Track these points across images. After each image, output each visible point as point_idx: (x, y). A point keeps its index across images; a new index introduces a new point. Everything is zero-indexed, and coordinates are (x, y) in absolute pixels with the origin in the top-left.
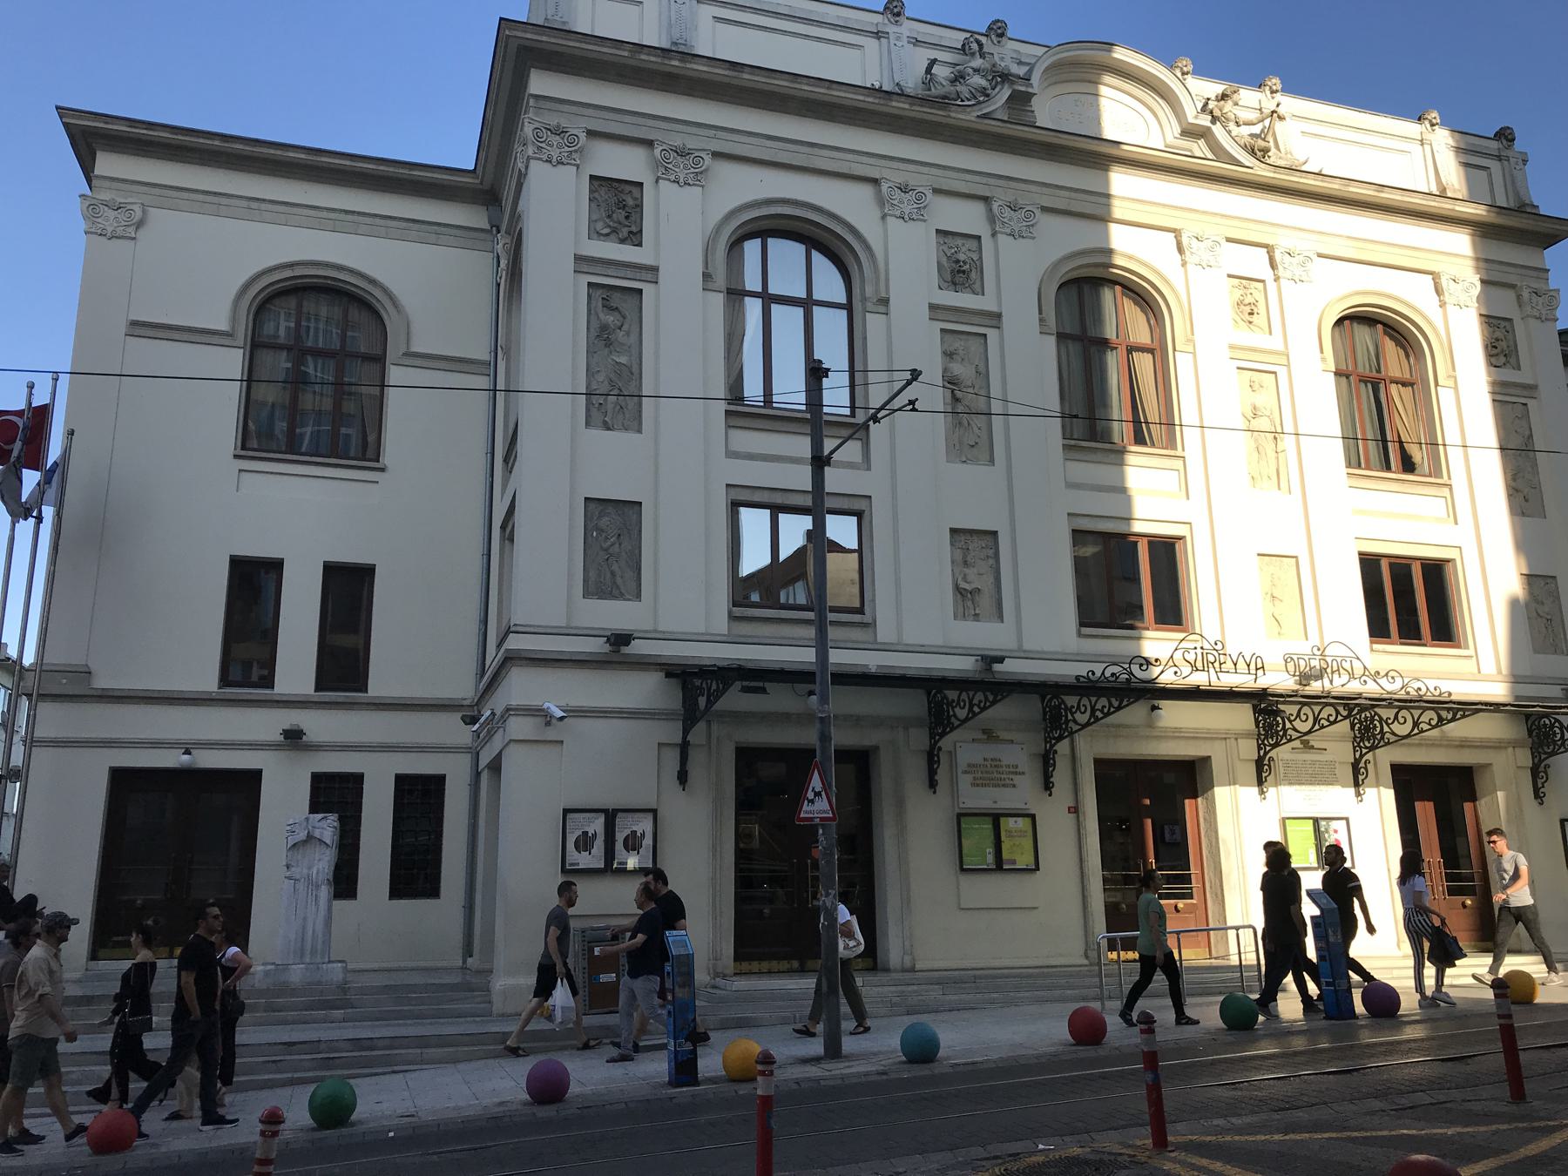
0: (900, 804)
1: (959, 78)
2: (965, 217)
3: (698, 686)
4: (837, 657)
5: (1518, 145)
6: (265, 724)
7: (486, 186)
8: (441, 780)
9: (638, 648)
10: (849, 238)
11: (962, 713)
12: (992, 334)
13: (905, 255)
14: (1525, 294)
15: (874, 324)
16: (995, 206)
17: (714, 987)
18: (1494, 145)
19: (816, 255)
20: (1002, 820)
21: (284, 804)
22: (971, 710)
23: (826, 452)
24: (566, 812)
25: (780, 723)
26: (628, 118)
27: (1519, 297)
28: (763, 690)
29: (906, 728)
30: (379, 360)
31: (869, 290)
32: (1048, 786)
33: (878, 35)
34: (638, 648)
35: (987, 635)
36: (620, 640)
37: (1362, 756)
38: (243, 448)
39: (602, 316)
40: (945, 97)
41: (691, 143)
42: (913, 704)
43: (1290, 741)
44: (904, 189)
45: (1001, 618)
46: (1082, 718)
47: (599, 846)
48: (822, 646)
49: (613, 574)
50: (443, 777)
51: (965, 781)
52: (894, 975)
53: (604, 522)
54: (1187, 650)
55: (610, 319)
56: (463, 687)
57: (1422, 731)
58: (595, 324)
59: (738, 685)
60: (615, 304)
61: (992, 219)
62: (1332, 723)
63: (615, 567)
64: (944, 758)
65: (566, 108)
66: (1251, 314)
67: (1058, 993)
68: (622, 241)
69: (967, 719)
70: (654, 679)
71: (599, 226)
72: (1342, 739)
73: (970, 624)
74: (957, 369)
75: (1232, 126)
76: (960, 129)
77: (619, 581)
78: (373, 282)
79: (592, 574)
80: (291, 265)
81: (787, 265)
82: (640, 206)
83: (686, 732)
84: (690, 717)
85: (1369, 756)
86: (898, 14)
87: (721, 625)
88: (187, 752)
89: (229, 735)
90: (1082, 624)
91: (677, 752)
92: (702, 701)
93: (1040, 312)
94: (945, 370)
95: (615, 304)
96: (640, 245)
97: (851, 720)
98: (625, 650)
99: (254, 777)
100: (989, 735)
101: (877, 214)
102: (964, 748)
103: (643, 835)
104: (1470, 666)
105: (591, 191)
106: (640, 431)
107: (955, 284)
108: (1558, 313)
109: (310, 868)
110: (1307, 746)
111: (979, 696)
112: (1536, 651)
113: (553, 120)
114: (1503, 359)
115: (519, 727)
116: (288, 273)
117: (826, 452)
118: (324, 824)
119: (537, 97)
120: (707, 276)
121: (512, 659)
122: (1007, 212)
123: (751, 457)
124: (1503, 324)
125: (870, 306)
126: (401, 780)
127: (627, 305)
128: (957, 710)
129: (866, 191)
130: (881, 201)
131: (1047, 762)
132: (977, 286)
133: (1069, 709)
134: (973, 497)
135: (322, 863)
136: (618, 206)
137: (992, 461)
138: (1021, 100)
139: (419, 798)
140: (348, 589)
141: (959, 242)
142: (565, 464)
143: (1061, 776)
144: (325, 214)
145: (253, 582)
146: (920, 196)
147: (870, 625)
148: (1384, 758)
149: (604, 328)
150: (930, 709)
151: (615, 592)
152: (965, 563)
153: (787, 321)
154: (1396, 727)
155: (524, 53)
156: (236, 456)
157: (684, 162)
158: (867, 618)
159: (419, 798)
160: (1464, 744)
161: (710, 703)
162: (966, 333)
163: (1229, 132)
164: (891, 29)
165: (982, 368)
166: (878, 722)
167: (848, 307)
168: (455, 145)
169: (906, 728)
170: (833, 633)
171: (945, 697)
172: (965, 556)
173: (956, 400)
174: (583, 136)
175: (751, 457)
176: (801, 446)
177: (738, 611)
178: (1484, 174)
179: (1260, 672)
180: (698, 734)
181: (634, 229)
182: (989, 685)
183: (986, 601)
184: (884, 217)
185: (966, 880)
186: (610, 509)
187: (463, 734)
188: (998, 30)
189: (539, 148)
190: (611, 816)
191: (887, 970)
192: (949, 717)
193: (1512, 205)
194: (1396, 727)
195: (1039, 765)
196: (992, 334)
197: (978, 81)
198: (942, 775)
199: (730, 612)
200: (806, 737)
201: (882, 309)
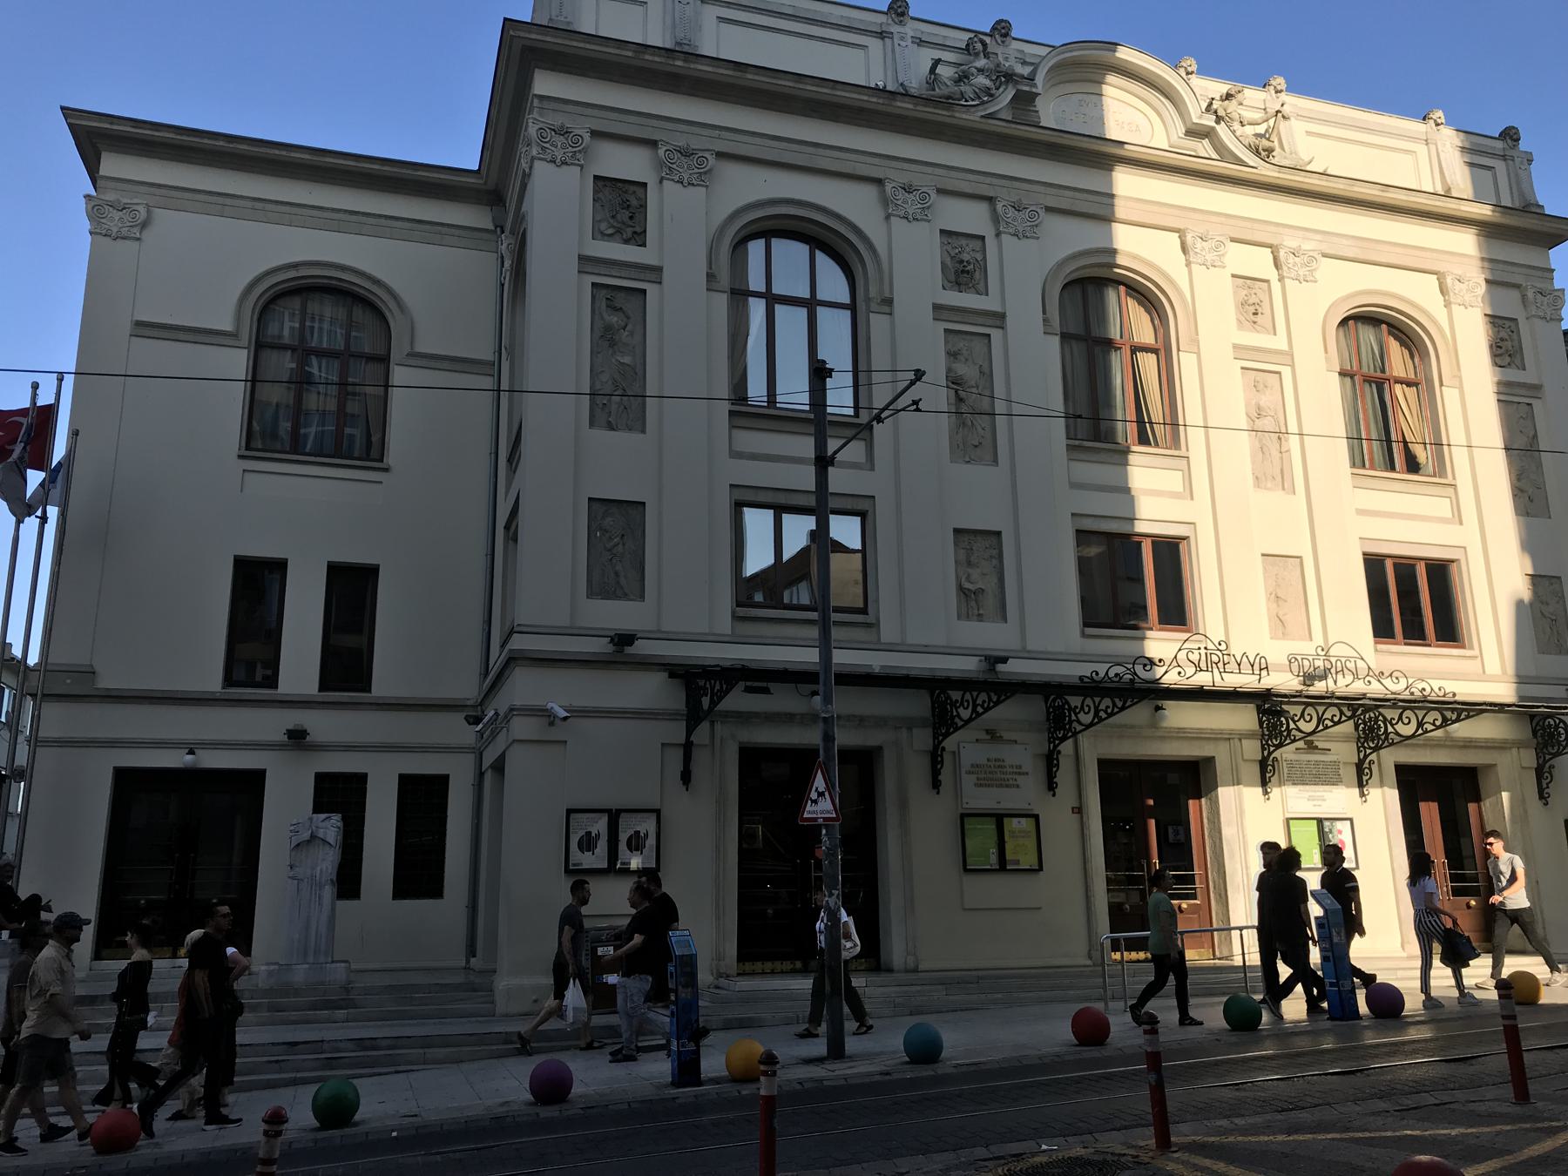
0: (903, 805)
3: (702, 687)
4: (841, 658)
6: (272, 724)
8: (444, 780)
9: (642, 648)
12: (996, 334)
13: (911, 258)
15: (878, 324)
16: (999, 206)
17: (717, 987)
18: (1499, 145)
19: (820, 255)
21: (287, 805)
22: (974, 710)
24: (569, 812)
26: (632, 119)
27: (994, 210)
28: (766, 691)
29: (910, 729)
30: (384, 360)
31: (873, 292)
32: (1051, 786)
34: (642, 648)
35: (990, 635)
36: (624, 640)
37: (1366, 756)
38: (248, 448)
39: (606, 316)
41: (695, 143)
42: (917, 705)
43: (1294, 741)
44: (908, 189)
46: (1086, 718)
49: (617, 574)
51: (968, 782)
54: (1191, 650)
55: (614, 319)
56: (467, 688)
57: (1426, 732)
59: (741, 685)
60: (619, 304)
61: (996, 219)
62: (1336, 724)
63: (619, 567)
64: (947, 758)
65: (570, 108)
68: (626, 242)
69: (970, 720)
71: (603, 226)
72: (1345, 739)
74: (961, 369)
77: (623, 581)
80: (295, 266)
81: (790, 264)
82: (644, 206)
83: (689, 732)
84: (694, 716)
85: (1373, 757)
87: (725, 625)
88: (191, 752)
89: (228, 737)
92: (706, 701)
94: (949, 370)
95: (619, 304)
98: (629, 650)
100: (993, 735)
102: (966, 746)
103: (598, 836)
104: (1473, 666)
106: (643, 431)
107: (959, 284)
110: (1311, 747)
113: (557, 120)
114: (1508, 359)
115: (521, 727)
116: (292, 274)
117: (830, 453)
119: (541, 98)
120: (711, 277)
124: (1508, 324)
125: (874, 306)
128: (961, 710)
129: (870, 191)
130: (885, 201)
131: (1051, 761)
132: (981, 287)
133: (954, 704)
136: (622, 207)
137: (995, 461)
138: (1025, 101)
139: (422, 799)
140: (352, 589)
141: (963, 242)
145: (257, 582)
146: (924, 196)
147: (873, 626)
148: (1389, 758)
149: (608, 328)
153: (791, 322)
154: (1400, 728)
155: (525, 52)
156: (240, 457)
157: (691, 162)
158: (870, 619)
160: (1468, 744)
161: (713, 703)
163: (1234, 132)
164: (895, 29)
165: (987, 371)
166: (881, 722)
167: (852, 307)
169: (910, 729)
170: (836, 633)
171: (949, 697)
173: (960, 400)
178: (1409, 157)
179: (1264, 673)
180: (702, 733)
181: (638, 229)
182: (993, 685)
183: (990, 601)
184: (888, 217)
185: (970, 880)
188: (1002, 29)
189: (544, 149)
190: (614, 816)
191: (890, 970)
192: (953, 718)
196: (996, 334)
197: (982, 80)
198: (946, 776)
199: (733, 613)
200: (811, 737)
201: (887, 309)
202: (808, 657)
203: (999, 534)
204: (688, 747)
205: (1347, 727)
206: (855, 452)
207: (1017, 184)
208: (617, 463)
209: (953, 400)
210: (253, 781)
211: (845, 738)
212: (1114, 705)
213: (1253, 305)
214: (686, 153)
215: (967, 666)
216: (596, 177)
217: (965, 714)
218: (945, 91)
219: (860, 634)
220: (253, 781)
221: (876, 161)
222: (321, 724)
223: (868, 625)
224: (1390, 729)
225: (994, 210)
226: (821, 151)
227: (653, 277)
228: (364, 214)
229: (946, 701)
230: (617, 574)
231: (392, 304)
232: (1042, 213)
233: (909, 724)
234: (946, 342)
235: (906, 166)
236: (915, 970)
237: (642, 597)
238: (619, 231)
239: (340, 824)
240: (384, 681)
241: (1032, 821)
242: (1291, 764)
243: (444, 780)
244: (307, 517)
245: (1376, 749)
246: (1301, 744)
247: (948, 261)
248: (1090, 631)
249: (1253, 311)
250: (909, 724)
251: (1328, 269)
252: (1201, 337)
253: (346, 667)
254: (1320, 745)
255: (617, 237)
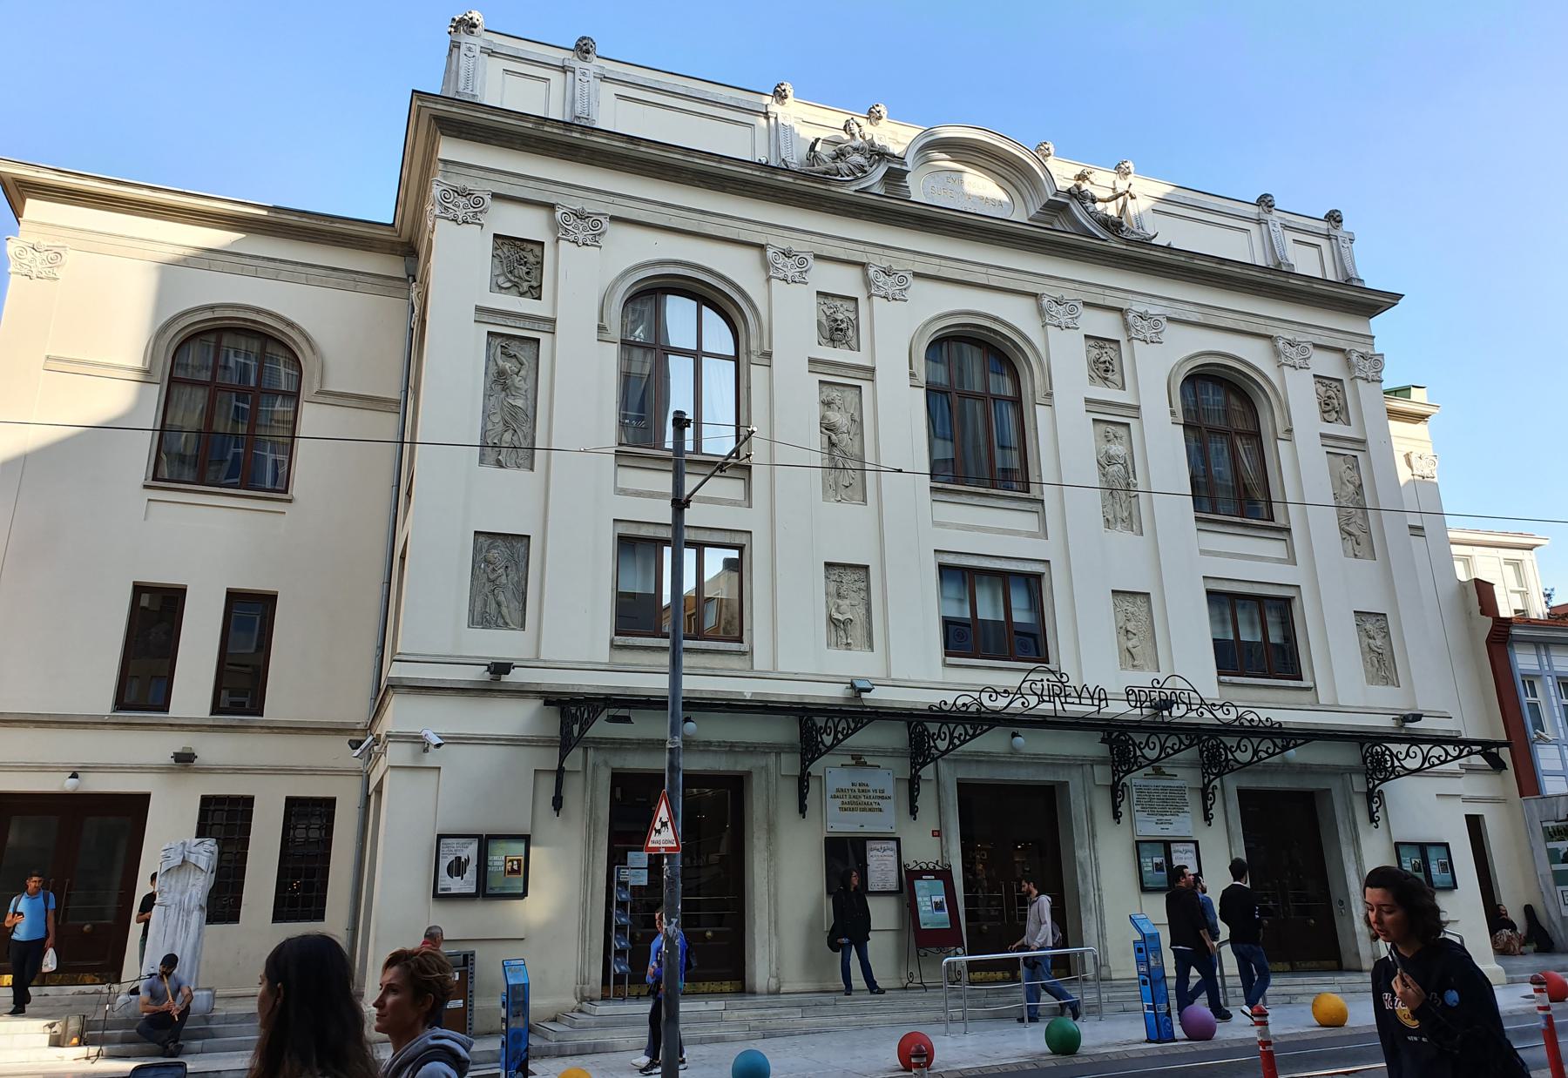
0: (771, 829)
1: (840, 155)
2: (845, 281)
3: (573, 712)
4: (689, 684)
5: (1346, 226)
6: (159, 746)
7: (404, 239)
8: (331, 802)
9: (515, 677)
10: (736, 297)
11: (828, 740)
12: (865, 385)
13: (790, 317)
14: (1354, 357)
15: (757, 374)
16: (871, 272)
17: (580, 1011)
18: (1324, 225)
19: (709, 314)
20: (1174, 847)
21: (170, 832)
22: (951, 742)
23: (687, 492)
24: (440, 837)
25: (647, 744)
26: (531, 183)
27: (1125, 320)
28: (627, 720)
29: (778, 754)
30: (294, 396)
31: (754, 345)
32: (913, 811)
33: (564, 69)
34: (515, 677)
35: (856, 664)
36: (500, 669)
37: (1210, 782)
38: (155, 478)
39: (500, 363)
40: (826, 173)
41: (590, 208)
42: (783, 731)
43: (1140, 767)
44: (787, 254)
45: (871, 647)
47: (471, 870)
48: (676, 672)
49: (499, 604)
50: (252, 798)
52: (759, 999)
53: (494, 553)
54: (1034, 682)
55: (508, 365)
56: (355, 711)
57: (1260, 759)
58: (493, 370)
60: (514, 352)
61: (868, 283)
62: (1176, 752)
63: (501, 598)
64: (813, 785)
65: (473, 172)
66: (1107, 371)
67: (913, 1016)
68: (522, 294)
69: (833, 746)
70: (533, 706)
71: (501, 280)
72: (1191, 765)
73: (843, 652)
74: (835, 417)
75: (1089, 204)
76: (839, 201)
77: (505, 610)
78: (291, 324)
79: (479, 604)
80: (212, 308)
81: (679, 315)
82: (540, 263)
83: (562, 759)
84: (566, 744)
85: (1217, 782)
86: (588, 52)
87: (603, 654)
88: (74, 776)
89: (119, 760)
90: (947, 654)
91: (552, 780)
92: (576, 728)
93: (601, 319)
94: (823, 418)
95: (514, 352)
96: (539, 298)
97: (709, 748)
98: (505, 678)
99: (142, 801)
100: (858, 761)
101: (762, 277)
102: (832, 772)
103: (467, 861)
104: (1306, 697)
105: (495, 249)
106: (532, 469)
107: (833, 340)
108: (1384, 375)
109: (182, 893)
110: (1159, 772)
111: (960, 730)
112: (1370, 681)
113: (460, 182)
115: (397, 754)
116: (209, 315)
117: (687, 492)
118: (201, 849)
119: (445, 162)
120: (601, 328)
121: (397, 686)
122: (882, 278)
123: (638, 494)
124: (1334, 384)
125: (754, 359)
126: (291, 802)
127: (525, 353)
128: (938, 742)
129: (751, 255)
130: (766, 265)
131: (913, 785)
132: (853, 343)
133: (931, 736)
134: (846, 532)
135: (198, 886)
136: (519, 262)
137: (865, 501)
138: (895, 177)
139: (309, 820)
140: (250, 615)
141: (838, 303)
142: (458, 498)
143: (1217, 810)
144: (248, 261)
146: (802, 262)
147: (748, 654)
148: (1232, 783)
149: (501, 373)
150: (911, 739)
151: (500, 622)
152: (839, 595)
154: (1238, 755)
155: (446, 119)
156: (145, 487)
157: (587, 226)
158: (745, 647)
159: (309, 820)
160: (1305, 769)
161: (582, 730)
162: (843, 384)
163: (1086, 209)
164: (579, 65)
165: (857, 418)
166: (751, 749)
167: (736, 359)
168: (375, 203)
169: (778, 754)
170: (687, 661)
171: (814, 724)
172: (838, 589)
173: (832, 444)
174: (488, 198)
175: (638, 494)
176: (665, 482)
177: (620, 640)
178: (1315, 250)
179: (1103, 704)
180: (575, 759)
181: (535, 284)
182: (856, 712)
183: (857, 632)
184: (769, 279)
186: (499, 542)
187: (352, 759)
189: (446, 208)
190: (485, 842)
191: (753, 993)
192: (817, 743)
193: (1340, 279)
194: (1238, 755)
195: (905, 787)
196: (865, 385)
197: (857, 159)
199: (612, 641)
200: (660, 763)
201: (766, 362)
202: (658, 683)
203: (867, 567)
204: (560, 773)
205: (1192, 753)
206: (721, 487)
207: (887, 252)
208: (505, 500)
209: (826, 444)
210: (139, 803)
211: (695, 763)
212: (1447, 753)
213: (1104, 362)
214: (580, 216)
215: (834, 693)
216: (496, 236)
217: (828, 740)
218: (822, 168)
219: (735, 663)
220: (139, 803)
221: (759, 228)
222: (211, 748)
223: (744, 653)
224: (1396, 763)
225: (1125, 320)
226: (708, 218)
227: (547, 327)
228: (281, 261)
229: (817, 727)
230: (499, 604)
231: (304, 346)
232: (1080, 307)
233: (777, 749)
234: (821, 392)
235: (786, 233)
236: (777, 992)
237: (523, 626)
238: (516, 285)
239: (215, 849)
240: (277, 705)
241: (1444, 849)
242: (1140, 790)
243: (331, 802)
244: (208, 545)
245: (1219, 775)
246: (1149, 770)
247: (824, 319)
248: (951, 660)
249: (1103, 370)
250: (777, 749)
251: (1171, 332)
252: (1055, 391)
253: (241, 687)
254: (1167, 771)
255: (514, 290)
